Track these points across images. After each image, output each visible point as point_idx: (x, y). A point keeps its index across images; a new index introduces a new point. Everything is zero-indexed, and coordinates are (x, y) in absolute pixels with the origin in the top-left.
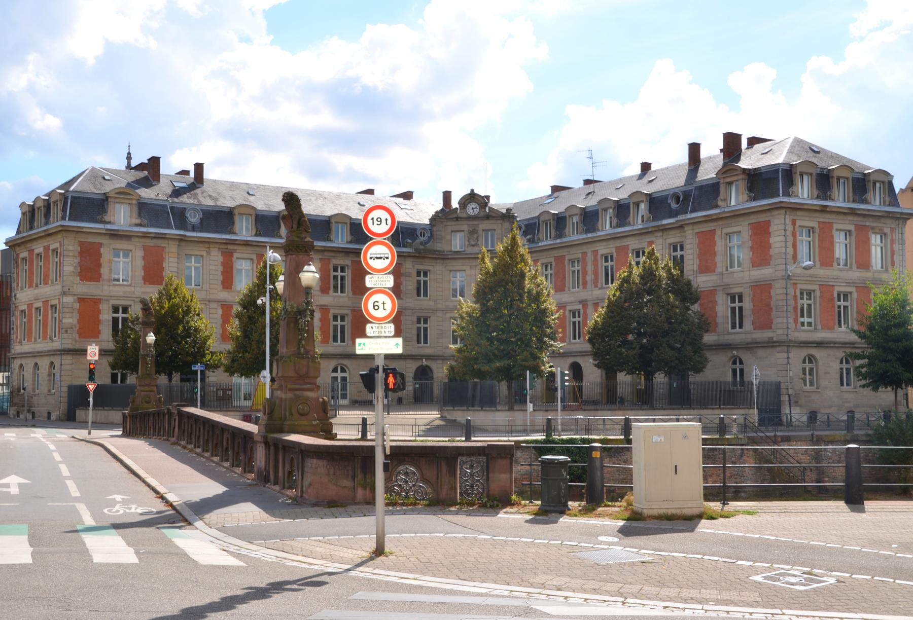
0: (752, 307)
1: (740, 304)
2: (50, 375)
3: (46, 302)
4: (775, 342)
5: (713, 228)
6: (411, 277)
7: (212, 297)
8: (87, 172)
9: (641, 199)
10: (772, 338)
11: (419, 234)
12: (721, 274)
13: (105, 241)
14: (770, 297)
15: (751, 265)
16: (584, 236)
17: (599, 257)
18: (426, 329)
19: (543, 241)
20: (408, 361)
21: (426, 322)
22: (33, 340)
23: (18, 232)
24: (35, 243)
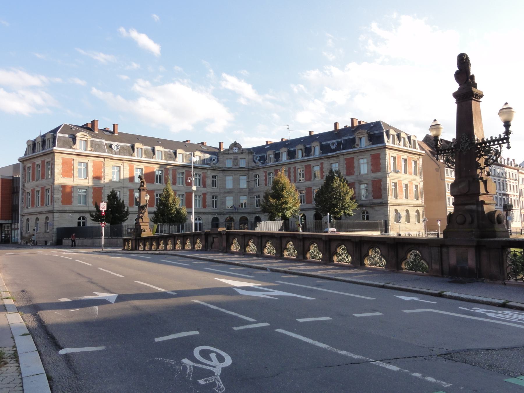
0: (372, 189)
1: (213, 200)
2: (45, 223)
3: (43, 188)
4: (384, 204)
5: (353, 157)
6: (210, 178)
7: (124, 186)
8: (63, 125)
9: (317, 145)
10: (382, 202)
11: (213, 160)
12: (357, 176)
13: (74, 157)
14: (381, 185)
15: (371, 172)
16: (290, 161)
17: (267, 174)
18: (216, 201)
19: (269, 163)
20: (210, 215)
21: (216, 198)
22: (35, 206)
23: (25, 154)
24: (36, 159)
